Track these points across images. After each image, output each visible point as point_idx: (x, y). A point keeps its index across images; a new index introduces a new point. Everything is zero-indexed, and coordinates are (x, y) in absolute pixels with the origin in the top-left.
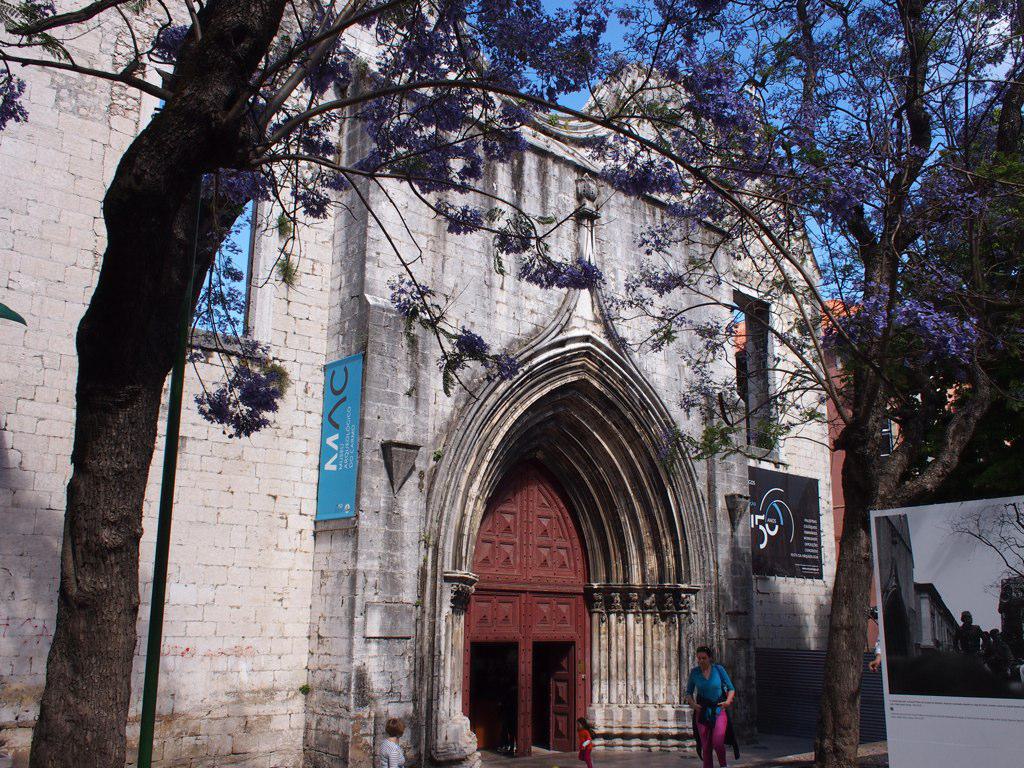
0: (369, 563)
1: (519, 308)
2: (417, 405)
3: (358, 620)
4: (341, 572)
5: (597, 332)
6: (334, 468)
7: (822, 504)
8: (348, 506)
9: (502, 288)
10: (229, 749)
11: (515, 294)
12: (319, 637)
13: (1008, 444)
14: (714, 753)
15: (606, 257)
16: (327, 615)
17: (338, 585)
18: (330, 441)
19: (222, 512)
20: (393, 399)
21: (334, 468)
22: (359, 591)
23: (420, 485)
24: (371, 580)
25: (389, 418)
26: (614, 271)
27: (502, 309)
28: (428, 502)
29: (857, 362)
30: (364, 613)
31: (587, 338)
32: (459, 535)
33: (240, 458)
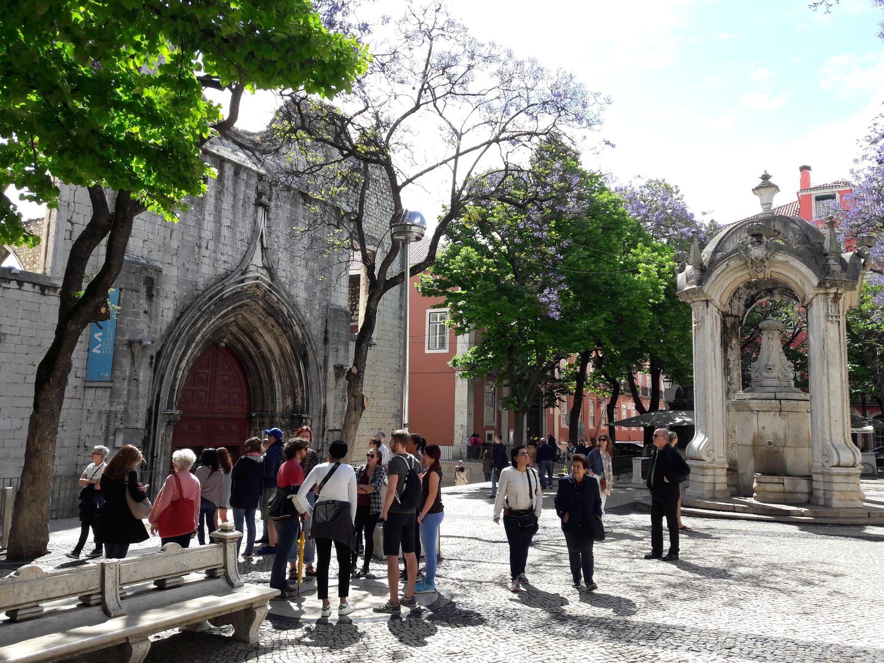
0: (118, 407)
1: (217, 260)
2: (151, 319)
3: (111, 438)
4: (100, 412)
5: (264, 274)
6: (99, 352)
7: (361, 283)
8: (107, 375)
9: (207, 248)
10: (203, 235)
11: (215, 251)
12: (86, 447)
13: (666, 481)
14: (334, 552)
15: (273, 228)
16: (91, 434)
17: (99, 418)
18: (96, 336)
19: (28, 377)
20: (136, 315)
21: (99, 352)
22: (112, 423)
23: (151, 363)
24: (119, 416)
25: (134, 326)
26: (278, 237)
27: (206, 261)
28: (155, 372)
29: (554, 455)
30: (114, 435)
31: (257, 278)
32: (172, 390)
33: (39, 345)
